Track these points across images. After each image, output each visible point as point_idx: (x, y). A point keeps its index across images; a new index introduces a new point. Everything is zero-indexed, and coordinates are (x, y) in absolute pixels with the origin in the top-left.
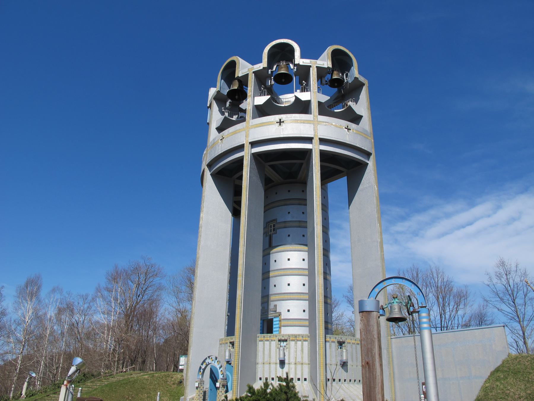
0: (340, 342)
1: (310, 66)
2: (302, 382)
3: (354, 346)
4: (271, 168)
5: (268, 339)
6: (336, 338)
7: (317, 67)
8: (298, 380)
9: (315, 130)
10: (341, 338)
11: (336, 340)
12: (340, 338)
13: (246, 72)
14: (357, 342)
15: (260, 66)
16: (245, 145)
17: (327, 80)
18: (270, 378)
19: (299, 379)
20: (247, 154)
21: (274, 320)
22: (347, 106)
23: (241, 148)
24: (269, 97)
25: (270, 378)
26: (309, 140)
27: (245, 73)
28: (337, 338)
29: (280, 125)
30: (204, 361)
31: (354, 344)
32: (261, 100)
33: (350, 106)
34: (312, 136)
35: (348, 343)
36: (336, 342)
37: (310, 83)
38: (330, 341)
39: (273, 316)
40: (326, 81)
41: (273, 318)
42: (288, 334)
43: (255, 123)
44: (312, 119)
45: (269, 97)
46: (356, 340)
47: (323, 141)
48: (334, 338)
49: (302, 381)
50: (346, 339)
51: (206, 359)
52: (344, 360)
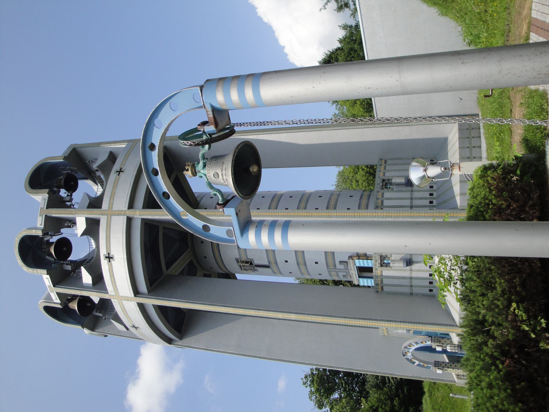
0: (375, 207)
1: (46, 216)
2: (435, 287)
3: (387, 168)
4: (174, 264)
5: (380, 287)
6: (378, 192)
7: (47, 208)
8: (433, 203)
9: (119, 213)
10: (378, 184)
11: (380, 191)
12: (379, 186)
13: (55, 294)
14: (383, 163)
15: (47, 278)
16: (138, 302)
17: (67, 194)
18: (430, 198)
19: (431, 195)
20: (151, 302)
21: (358, 265)
22: (99, 170)
23: (142, 307)
24: (82, 268)
25: (430, 198)
26: (129, 220)
27: (55, 296)
28: (378, 189)
29: (112, 258)
30: (411, 361)
31: (385, 167)
32: (87, 278)
33: (97, 167)
34: (125, 217)
35: (384, 175)
36: (383, 191)
37: (66, 217)
38: (382, 199)
39: (354, 266)
40: (68, 195)
41: (356, 267)
42: (393, 192)
43: (112, 288)
44: (106, 217)
45: (83, 268)
46: (381, 165)
47: (131, 206)
48: (378, 193)
49: (430, 198)
50: (379, 177)
51: (408, 359)
52: (405, 182)
